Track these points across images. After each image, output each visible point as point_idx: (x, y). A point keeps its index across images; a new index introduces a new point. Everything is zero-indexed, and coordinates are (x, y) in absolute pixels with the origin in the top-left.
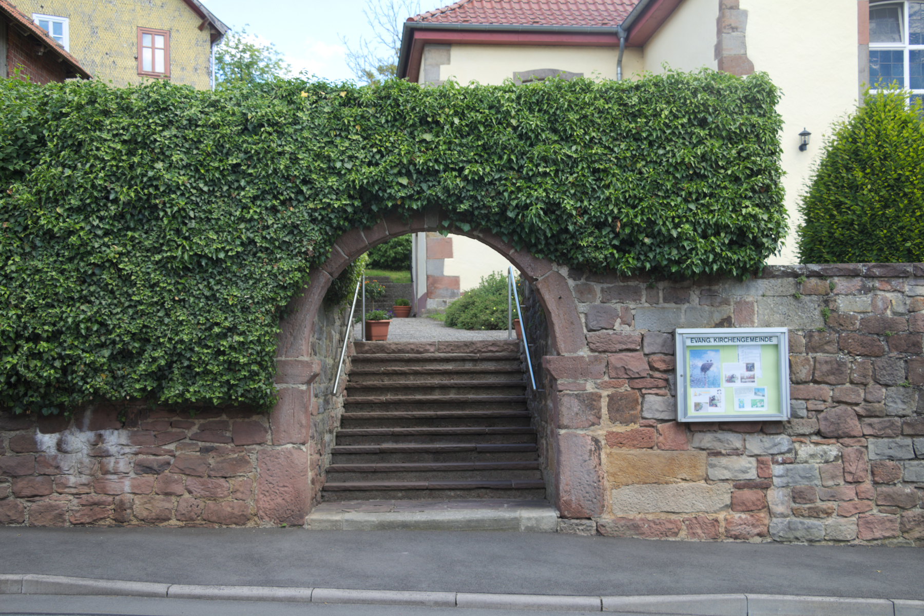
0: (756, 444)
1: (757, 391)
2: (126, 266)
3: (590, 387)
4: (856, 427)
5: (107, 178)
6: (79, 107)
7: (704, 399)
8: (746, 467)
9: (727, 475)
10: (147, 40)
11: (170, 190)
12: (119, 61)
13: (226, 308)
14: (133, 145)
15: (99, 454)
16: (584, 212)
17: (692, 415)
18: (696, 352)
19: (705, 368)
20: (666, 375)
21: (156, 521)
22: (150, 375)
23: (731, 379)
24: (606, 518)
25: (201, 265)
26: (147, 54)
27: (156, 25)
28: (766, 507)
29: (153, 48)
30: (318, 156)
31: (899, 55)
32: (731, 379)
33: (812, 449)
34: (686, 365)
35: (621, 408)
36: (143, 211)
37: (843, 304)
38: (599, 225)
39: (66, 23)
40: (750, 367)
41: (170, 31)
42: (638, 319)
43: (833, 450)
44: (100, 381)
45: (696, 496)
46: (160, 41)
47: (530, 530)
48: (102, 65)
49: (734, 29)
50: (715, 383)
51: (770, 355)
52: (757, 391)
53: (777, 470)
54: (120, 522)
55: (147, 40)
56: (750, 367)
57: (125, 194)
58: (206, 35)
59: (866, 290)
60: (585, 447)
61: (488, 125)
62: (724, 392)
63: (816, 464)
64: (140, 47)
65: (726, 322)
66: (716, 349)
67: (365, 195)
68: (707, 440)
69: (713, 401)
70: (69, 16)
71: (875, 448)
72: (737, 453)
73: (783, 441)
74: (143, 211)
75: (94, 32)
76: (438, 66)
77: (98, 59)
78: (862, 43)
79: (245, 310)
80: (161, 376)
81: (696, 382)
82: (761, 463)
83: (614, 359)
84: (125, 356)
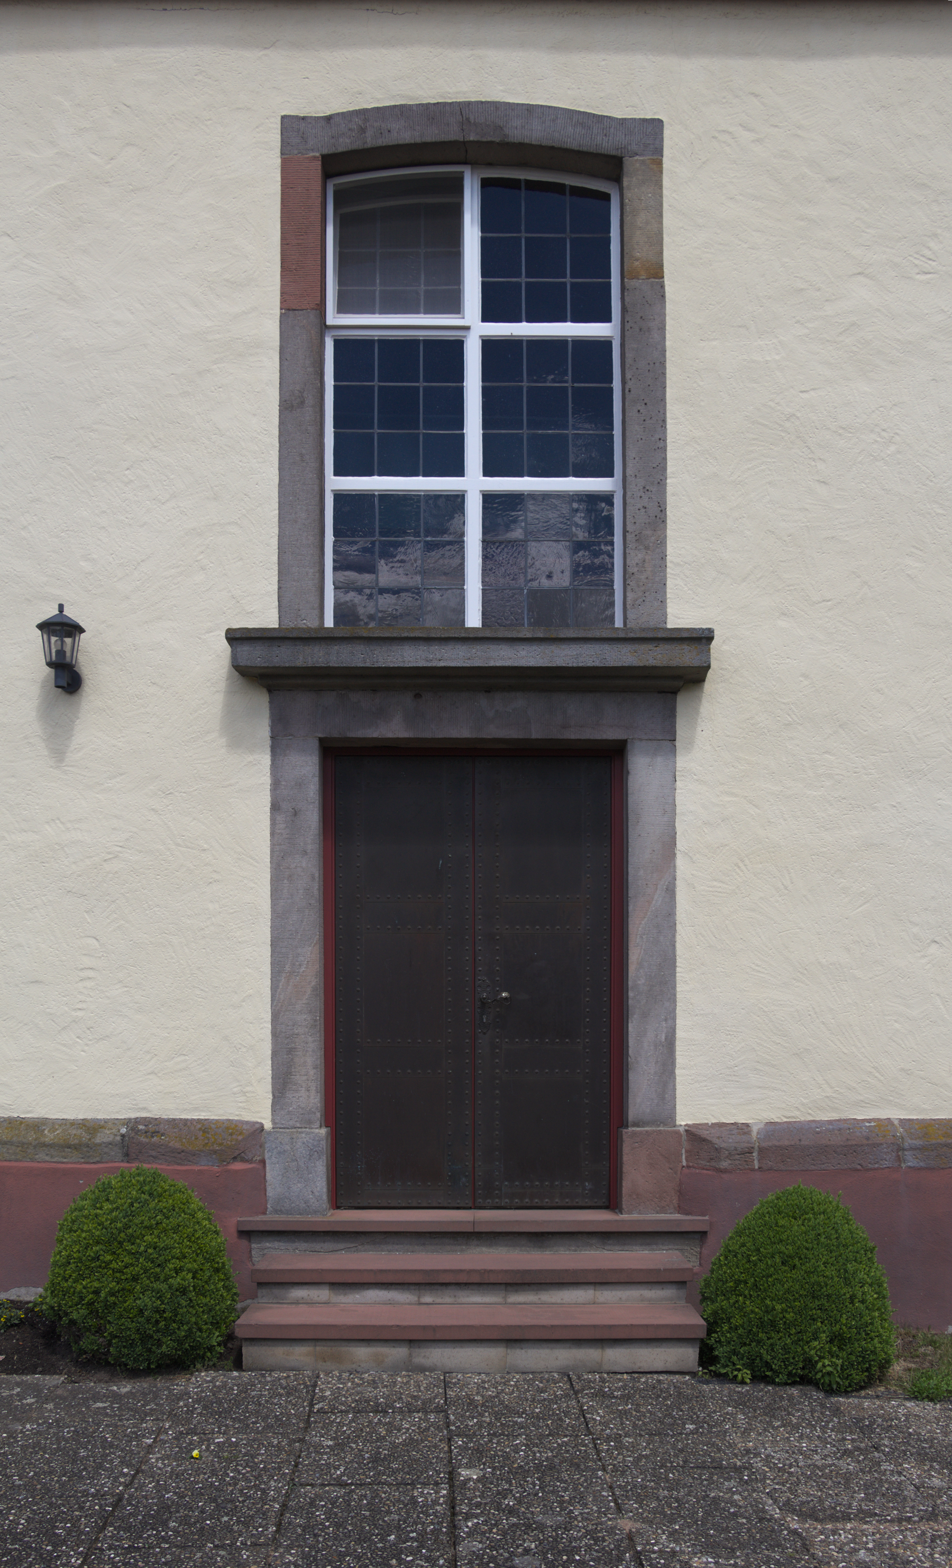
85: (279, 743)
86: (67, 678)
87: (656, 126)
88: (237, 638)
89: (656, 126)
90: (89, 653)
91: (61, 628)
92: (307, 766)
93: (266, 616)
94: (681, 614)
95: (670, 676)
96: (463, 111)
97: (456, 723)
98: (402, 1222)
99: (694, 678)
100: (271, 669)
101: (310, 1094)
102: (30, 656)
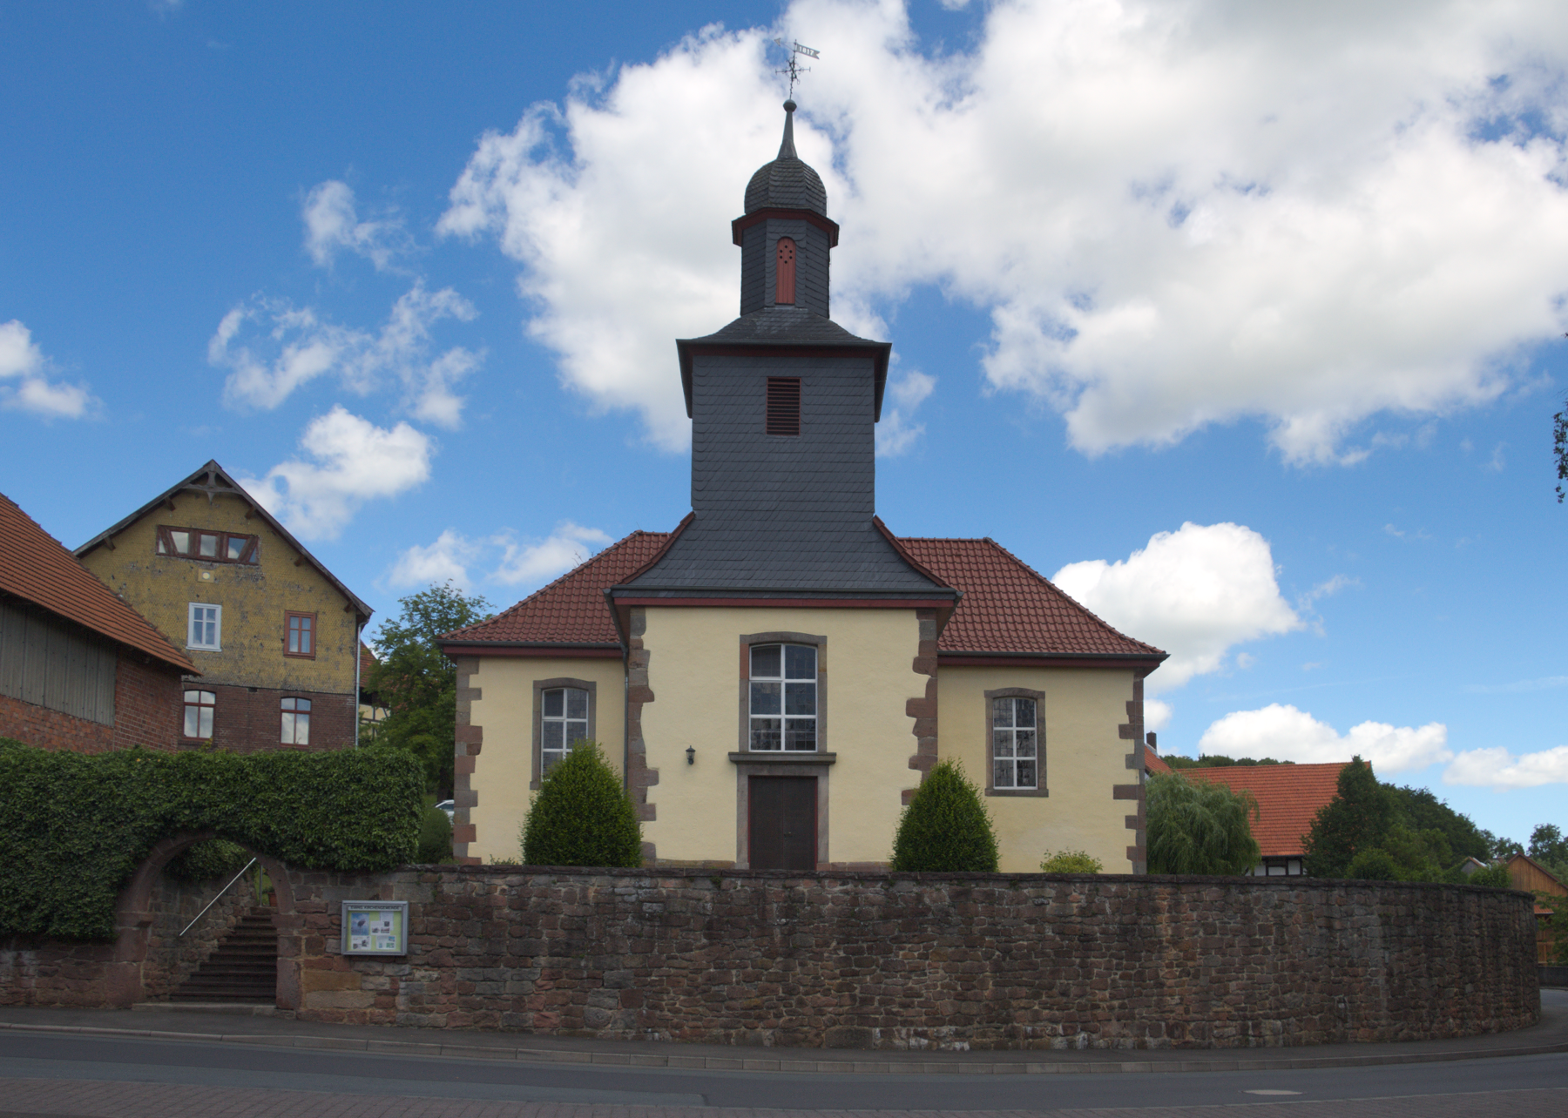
0: (390, 970)
1: (391, 938)
2: (30, 858)
3: (295, 933)
4: (452, 961)
5: (22, 808)
6: (15, 767)
7: (359, 942)
8: (384, 982)
9: (372, 986)
10: (295, 623)
11: (54, 815)
12: (267, 643)
13: (82, 882)
14: (39, 789)
15: (18, 964)
16: (284, 831)
17: (351, 950)
18: (356, 914)
19: (361, 924)
20: (336, 930)
21: (48, 1004)
22: (41, 919)
23: (375, 931)
24: (302, 1010)
25: (69, 858)
26: (294, 636)
27: (303, 608)
28: (394, 1006)
29: (300, 631)
30: (139, 798)
31: (560, 725)
32: (375, 931)
33: (423, 973)
34: (350, 922)
35: (315, 946)
36: (39, 828)
37: (446, 888)
38: (295, 840)
39: (219, 609)
40: (387, 924)
41: (316, 614)
42: (322, 895)
43: (435, 975)
44: (14, 922)
45: (354, 999)
46: (307, 624)
47: (258, 1015)
48: (250, 647)
49: (639, 665)
50: (366, 933)
51: (398, 918)
52: (391, 938)
53: (402, 985)
54: (29, 1004)
55: (295, 623)
56: (387, 924)
57: (30, 817)
58: (352, 617)
59: (462, 881)
60: (293, 968)
61: (235, 780)
62: (370, 938)
63: (425, 982)
64: (287, 629)
65: (376, 897)
66: (368, 913)
67: (168, 820)
68: (361, 966)
69: (364, 944)
70: (221, 603)
71: (460, 974)
72: (379, 974)
73: (407, 968)
74: (39, 828)
75: (244, 617)
76: (468, 675)
77: (246, 642)
78: (744, 677)
79: (94, 883)
80: (47, 919)
81: (355, 932)
82: (393, 980)
83: (309, 917)
84: (28, 908)
85: (739, 773)
86: (691, 761)
87: (824, 638)
88: (730, 754)
89: (824, 638)
90: (697, 756)
91: (691, 751)
92: (745, 781)
93: (736, 750)
94: (830, 749)
95: (828, 762)
96: (781, 634)
97: (779, 772)
98: (695, 480)
99: (833, 762)
100: (738, 760)
101: (745, 855)
102: (684, 756)
